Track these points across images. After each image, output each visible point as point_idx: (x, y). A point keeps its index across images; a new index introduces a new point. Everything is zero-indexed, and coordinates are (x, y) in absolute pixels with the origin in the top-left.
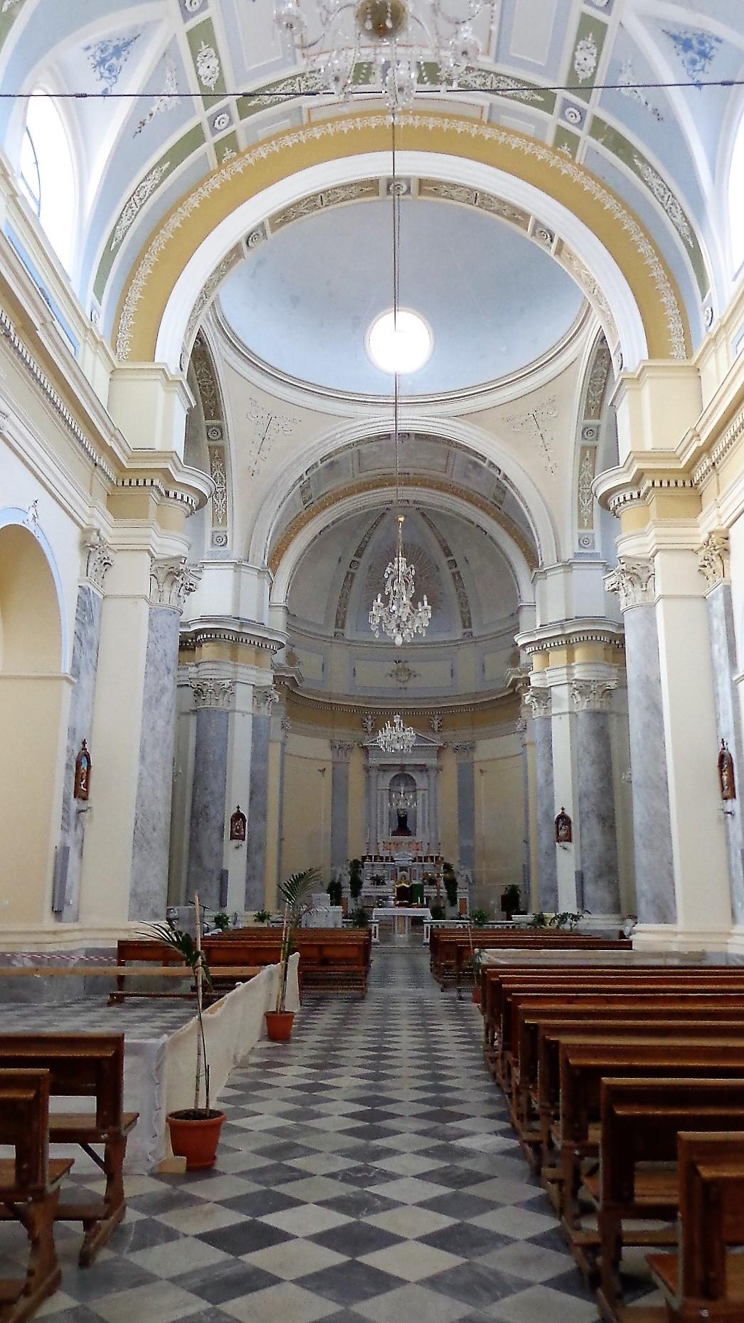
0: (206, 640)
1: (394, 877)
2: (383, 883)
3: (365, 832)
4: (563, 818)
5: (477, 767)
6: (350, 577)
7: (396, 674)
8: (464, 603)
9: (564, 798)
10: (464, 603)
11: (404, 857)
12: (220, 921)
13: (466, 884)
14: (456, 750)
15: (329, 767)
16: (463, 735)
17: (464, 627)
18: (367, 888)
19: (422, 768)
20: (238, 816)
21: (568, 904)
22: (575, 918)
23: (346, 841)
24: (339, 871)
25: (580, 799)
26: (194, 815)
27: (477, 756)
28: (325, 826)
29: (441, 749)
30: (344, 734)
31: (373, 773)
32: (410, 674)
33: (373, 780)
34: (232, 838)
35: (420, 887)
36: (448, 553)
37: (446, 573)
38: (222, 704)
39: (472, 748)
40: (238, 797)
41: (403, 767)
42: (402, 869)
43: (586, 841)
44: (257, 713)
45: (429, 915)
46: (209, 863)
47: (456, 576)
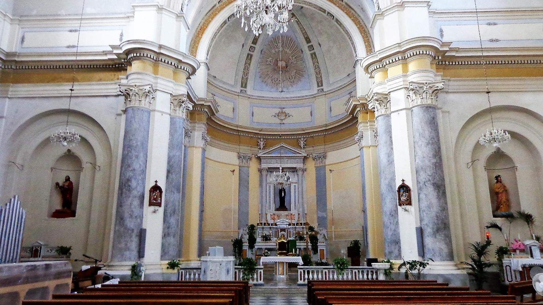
0: (135, 58)
1: (277, 236)
2: (270, 240)
3: (260, 206)
4: (404, 188)
5: (328, 168)
6: (250, 57)
8: (318, 73)
9: (404, 172)
10: (318, 73)
11: (283, 222)
12: (135, 269)
13: (323, 240)
14: (314, 159)
15: (237, 169)
16: (319, 149)
17: (318, 86)
18: (259, 243)
19: (294, 170)
20: (156, 188)
21: (410, 252)
22: (131, 216)
23: (247, 213)
24: (241, 231)
25: (417, 172)
26: (120, 189)
27: (328, 161)
28: (234, 206)
29: (305, 158)
30: (245, 149)
31: (264, 173)
32: (287, 115)
33: (264, 177)
34: (151, 204)
35: (293, 243)
36: (308, 40)
37: (307, 53)
38: (144, 103)
39: (325, 157)
40: (157, 173)
42: (283, 230)
43: (424, 204)
44: (173, 114)
45: (301, 262)
46: (130, 223)
47: (314, 56)
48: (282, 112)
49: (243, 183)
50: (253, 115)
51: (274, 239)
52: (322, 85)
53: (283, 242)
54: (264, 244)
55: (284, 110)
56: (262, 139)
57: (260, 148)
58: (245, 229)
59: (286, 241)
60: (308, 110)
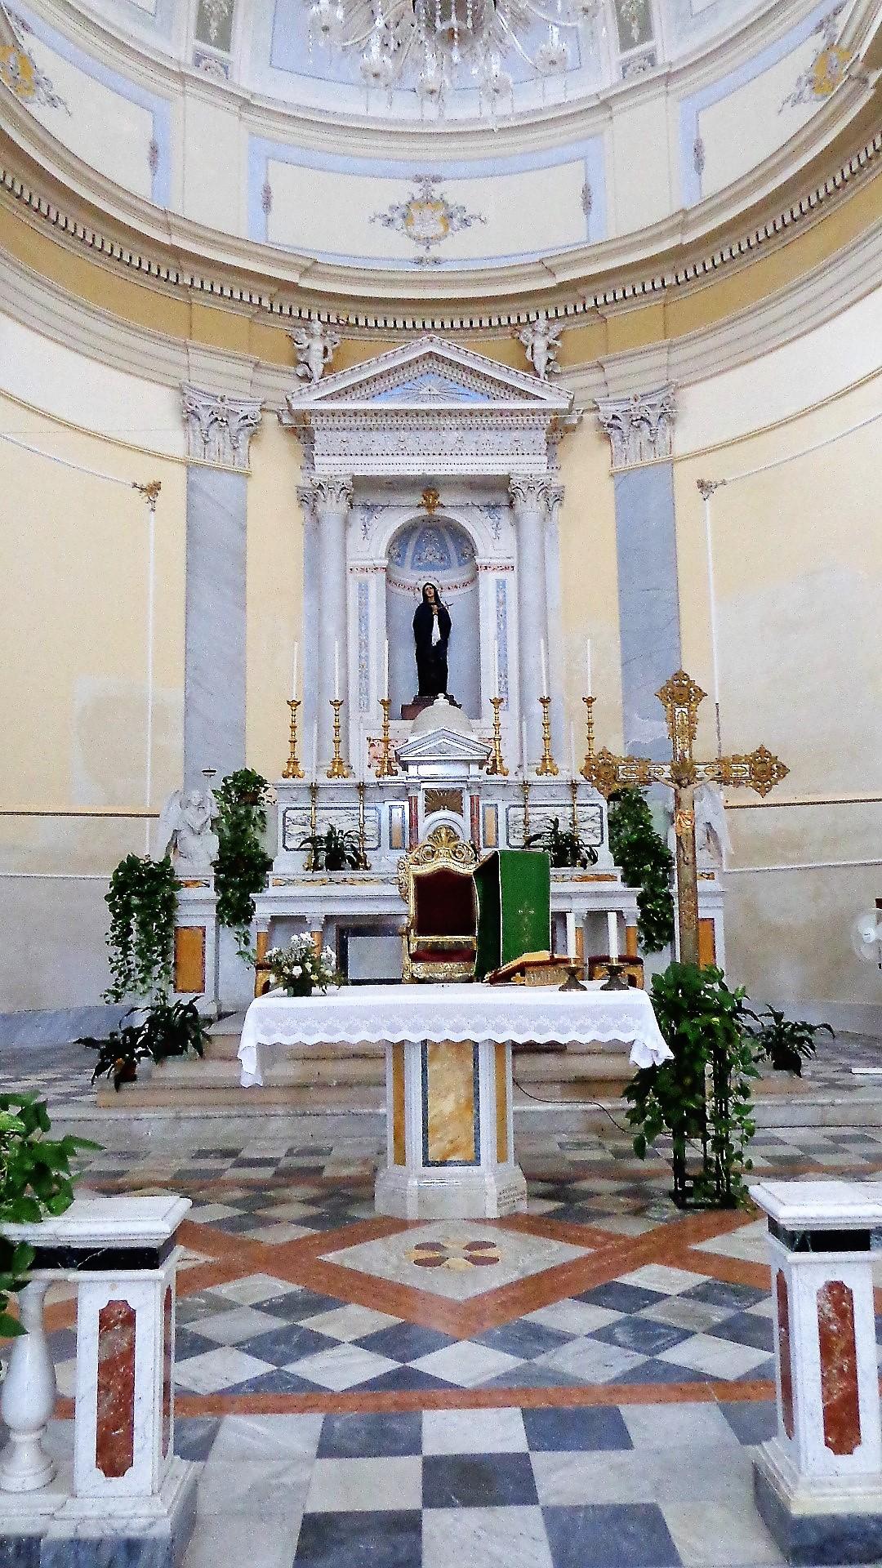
2: (359, 862)
5: (685, 477)
7: (406, 214)
14: (608, 430)
15: (174, 481)
16: (635, 375)
17: (626, 43)
18: (291, 887)
19: (497, 493)
27: (684, 439)
28: (162, 683)
30: (221, 374)
33: (331, 528)
39: (668, 416)
41: (429, 488)
42: (440, 799)
48: (428, 201)
49: (213, 560)
50: (267, 204)
51: (384, 860)
52: (646, 32)
53: (444, 875)
54: (313, 890)
55: (437, 190)
56: (317, 327)
57: (307, 378)
58: (195, 796)
59: (469, 870)
60: (567, 182)
